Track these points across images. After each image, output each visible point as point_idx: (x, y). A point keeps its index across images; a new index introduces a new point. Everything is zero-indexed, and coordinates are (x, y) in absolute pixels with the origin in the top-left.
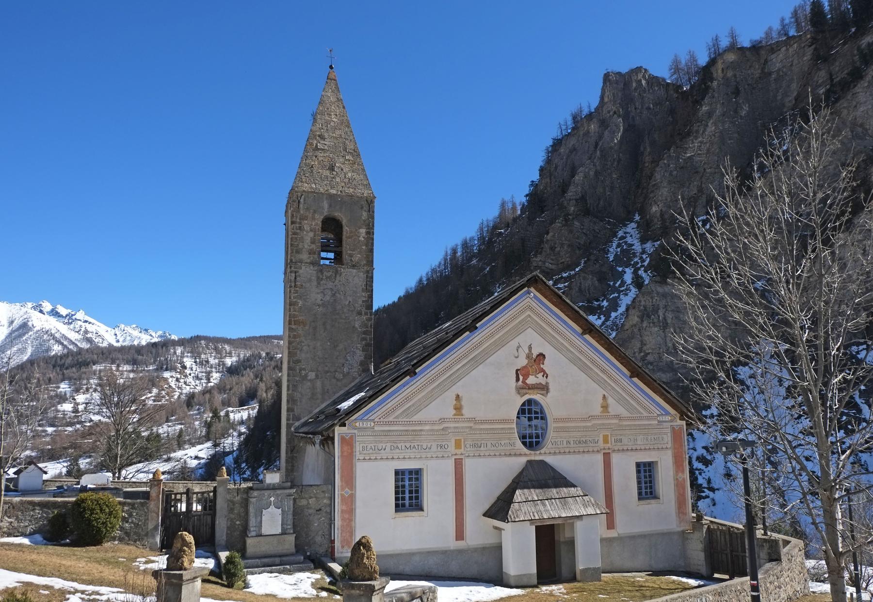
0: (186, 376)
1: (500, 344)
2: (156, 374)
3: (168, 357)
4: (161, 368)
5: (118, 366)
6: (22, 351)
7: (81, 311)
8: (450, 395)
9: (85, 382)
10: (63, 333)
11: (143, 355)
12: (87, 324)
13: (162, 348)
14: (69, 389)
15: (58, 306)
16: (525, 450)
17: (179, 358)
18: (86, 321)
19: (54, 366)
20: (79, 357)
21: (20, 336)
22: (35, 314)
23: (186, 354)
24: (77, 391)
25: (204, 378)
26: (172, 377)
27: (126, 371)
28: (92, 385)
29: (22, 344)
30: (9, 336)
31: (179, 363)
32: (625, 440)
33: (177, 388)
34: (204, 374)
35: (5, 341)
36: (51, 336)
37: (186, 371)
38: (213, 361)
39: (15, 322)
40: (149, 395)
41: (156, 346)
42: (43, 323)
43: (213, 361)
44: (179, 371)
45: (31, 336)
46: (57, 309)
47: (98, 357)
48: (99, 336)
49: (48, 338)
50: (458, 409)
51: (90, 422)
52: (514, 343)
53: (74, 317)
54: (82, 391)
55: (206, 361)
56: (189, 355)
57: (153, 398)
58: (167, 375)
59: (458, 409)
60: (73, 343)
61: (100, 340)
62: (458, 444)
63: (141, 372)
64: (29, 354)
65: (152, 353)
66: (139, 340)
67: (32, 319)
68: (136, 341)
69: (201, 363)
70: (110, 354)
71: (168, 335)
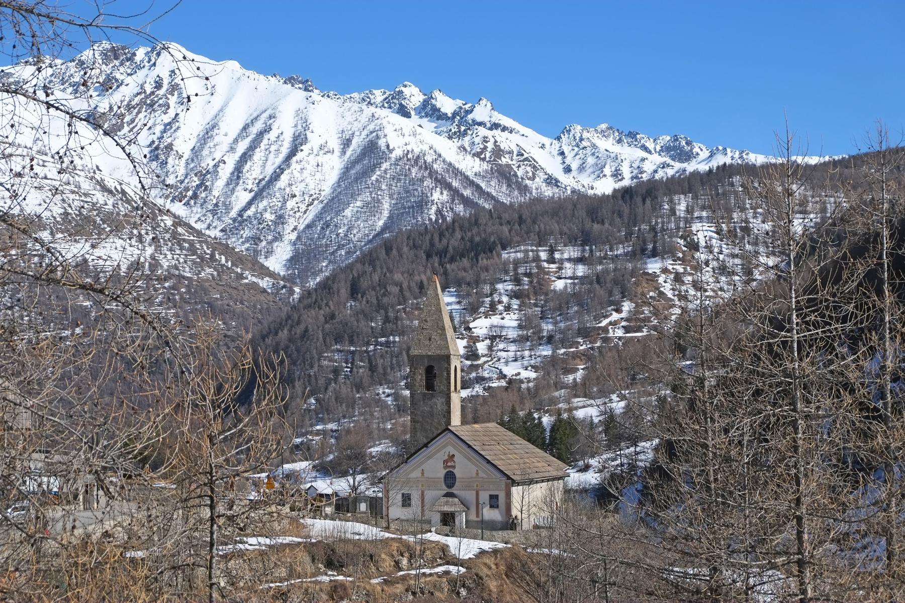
0: (697, 268)
1: (439, 451)
2: (630, 266)
3: (657, 223)
4: (642, 252)
5: (552, 251)
6: (372, 207)
7: (484, 102)
8: (420, 469)
9: (487, 288)
10: (448, 160)
11: (603, 223)
12: (497, 132)
13: (644, 201)
14: (457, 307)
15: (437, 94)
16: (446, 488)
17: (682, 225)
18: (495, 126)
19: (429, 256)
20: (475, 230)
21: (366, 173)
22: (391, 120)
23: (696, 214)
24: (473, 310)
25: (738, 269)
26: (665, 271)
27: (569, 260)
28: (500, 294)
29: (371, 193)
30: (344, 173)
31: (681, 238)
32: (485, 486)
33: (676, 298)
34: (737, 261)
35: (339, 186)
36: (426, 168)
37: (697, 255)
38: (760, 226)
39: (354, 142)
40: (615, 316)
41: (631, 197)
42: (407, 139)
43: (760, 226)
44: (680, 255)
45: (385, 171)
46: (433, 101)
47: (510, 231)
48: (526, 159)
49: (419, 175)
50: (423, 474)
51: (498, 379)
52: (444, 451)
53: (470, 117)
54: (482, 310)
55: (742, 228)
56: (704, 214)
57: (624, 323)
58: (654, 266)
59: (423, 474)
60: (472, 183)
61: (529, 169)
62: (422, 486)
63: (600, 261)
64: (386, 214)
65: (620, 216)
66: (615, 165)
67: (386, 131)
68: (607, 166)
69: (732, 234)
70: (534, 222)
71: (683, 143)
